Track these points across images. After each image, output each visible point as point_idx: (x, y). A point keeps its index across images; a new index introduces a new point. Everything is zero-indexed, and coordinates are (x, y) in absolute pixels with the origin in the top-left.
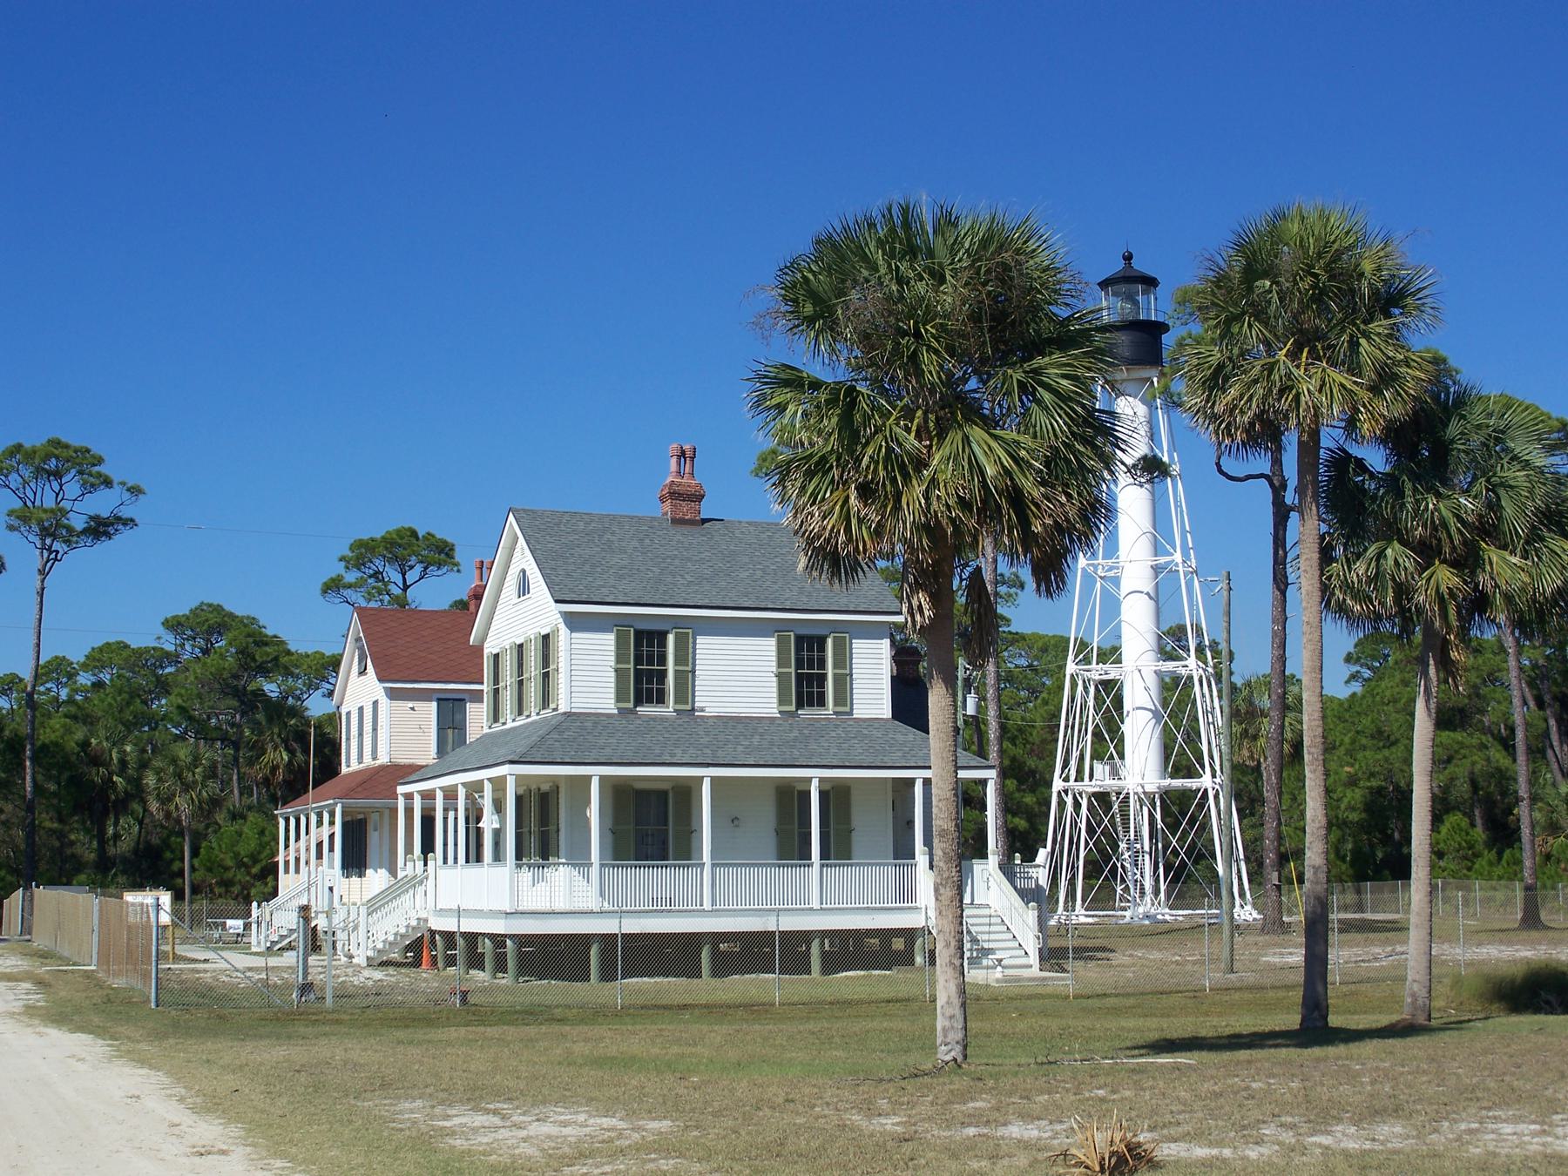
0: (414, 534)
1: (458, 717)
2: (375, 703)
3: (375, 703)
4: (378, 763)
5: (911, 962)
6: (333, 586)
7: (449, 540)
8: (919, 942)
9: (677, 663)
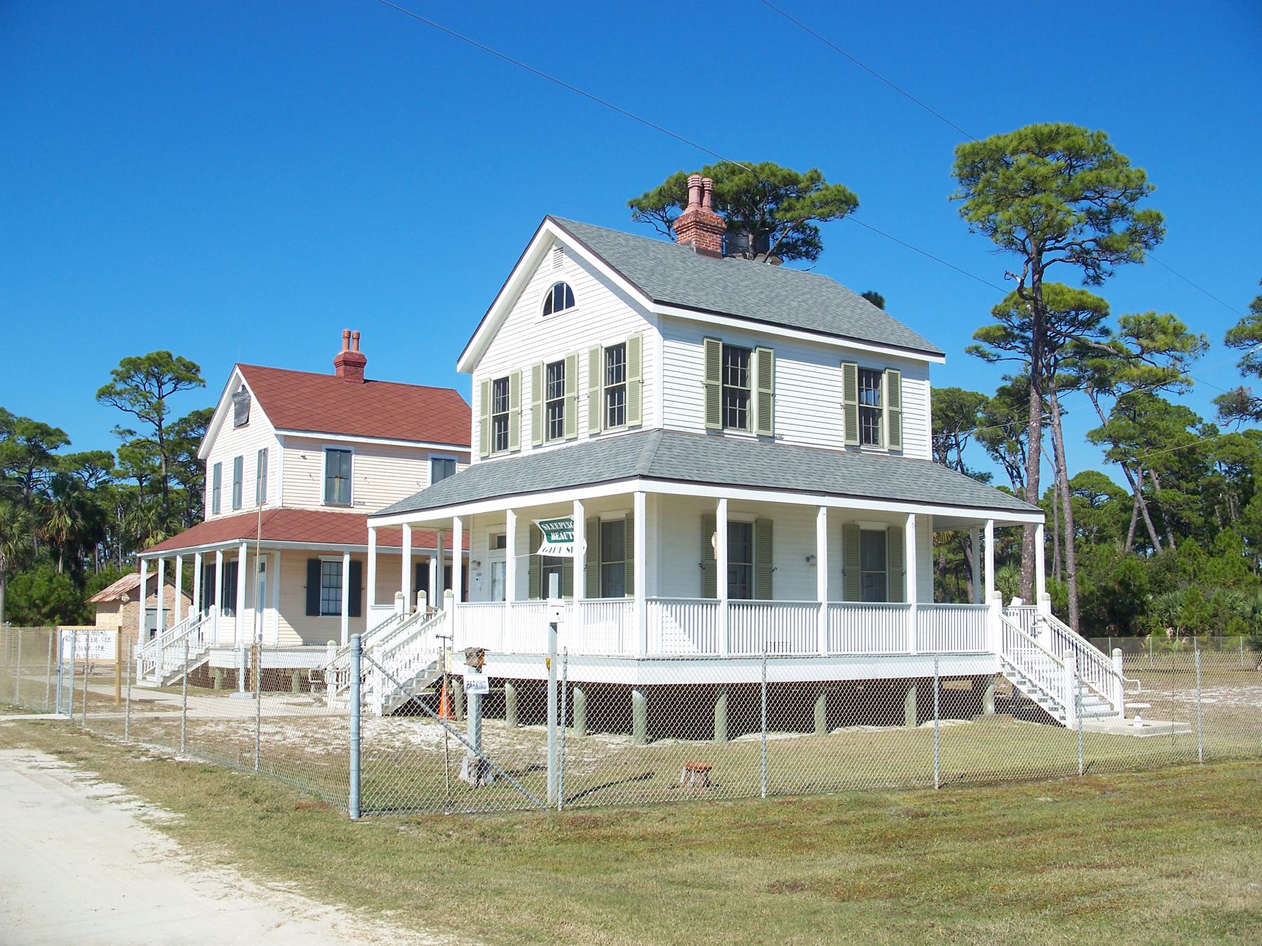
0: (170, 356)
1: (344, 467)
2: (263, 453)
3: (263, 453)
4: (220, 516)
5: (979, 709)
6: (106, 393)
7: (197, 364)
8: (990, 690)
9: (760, 385)
